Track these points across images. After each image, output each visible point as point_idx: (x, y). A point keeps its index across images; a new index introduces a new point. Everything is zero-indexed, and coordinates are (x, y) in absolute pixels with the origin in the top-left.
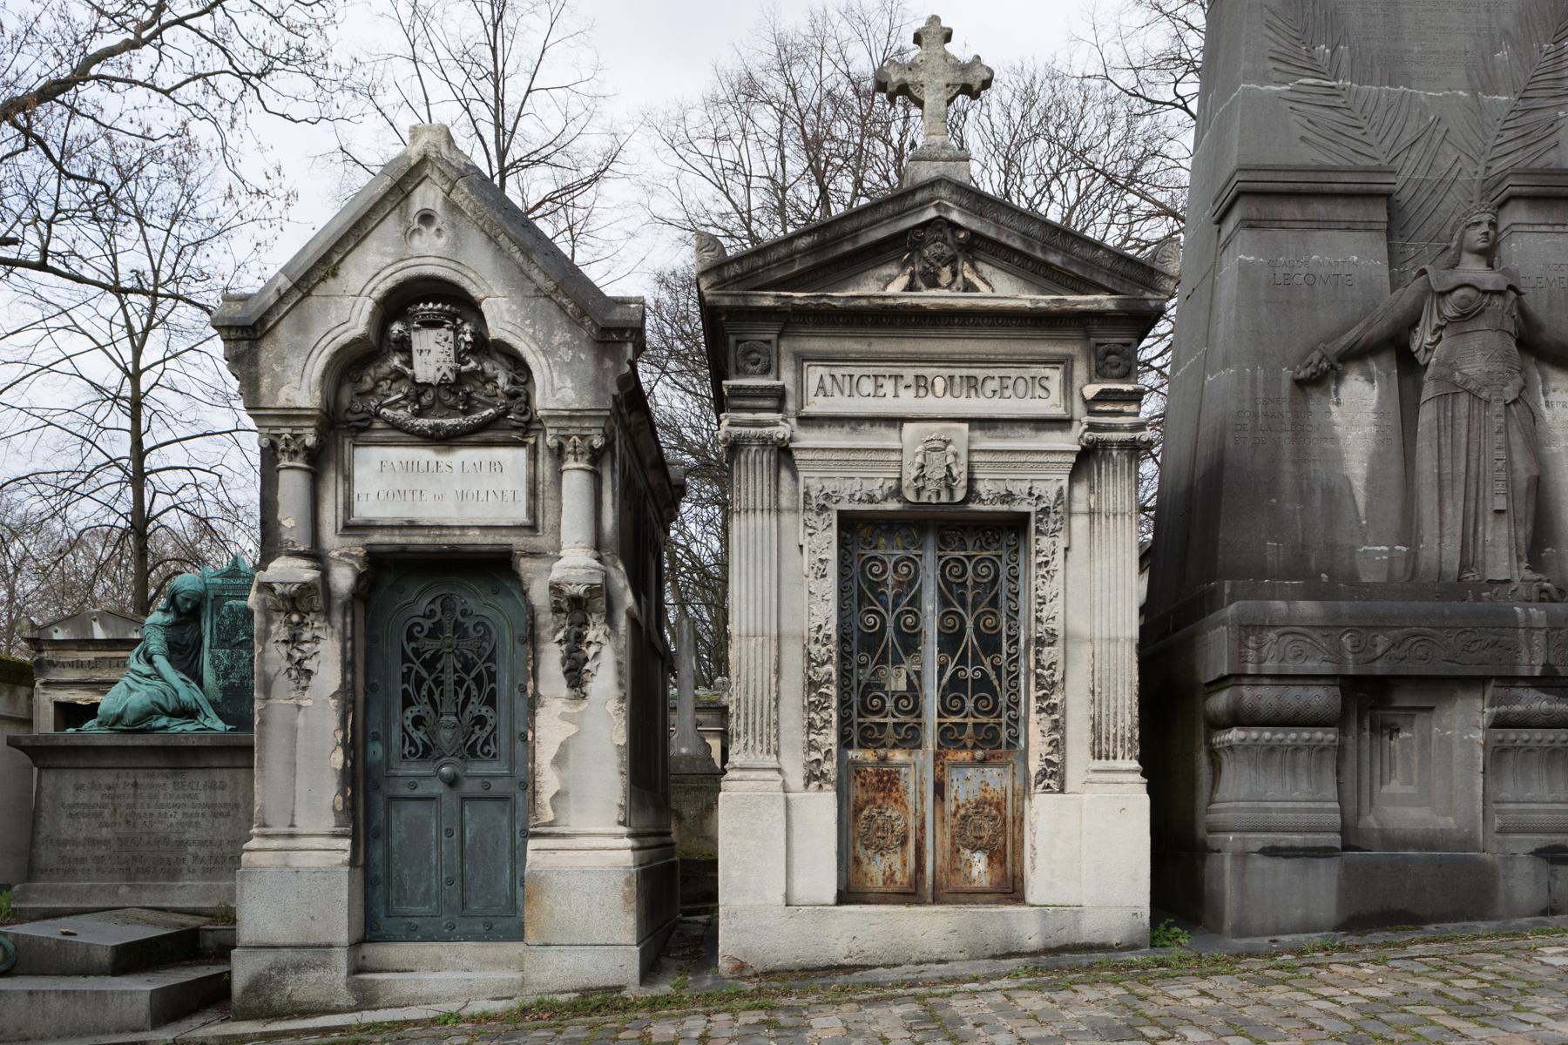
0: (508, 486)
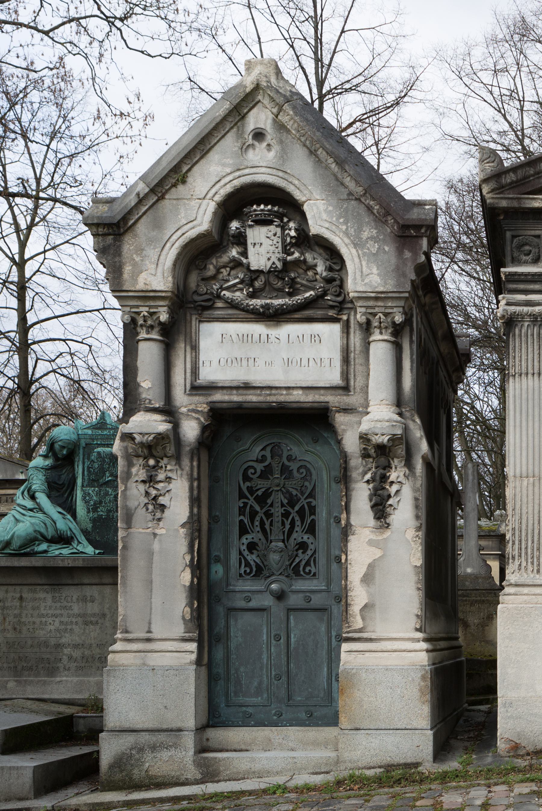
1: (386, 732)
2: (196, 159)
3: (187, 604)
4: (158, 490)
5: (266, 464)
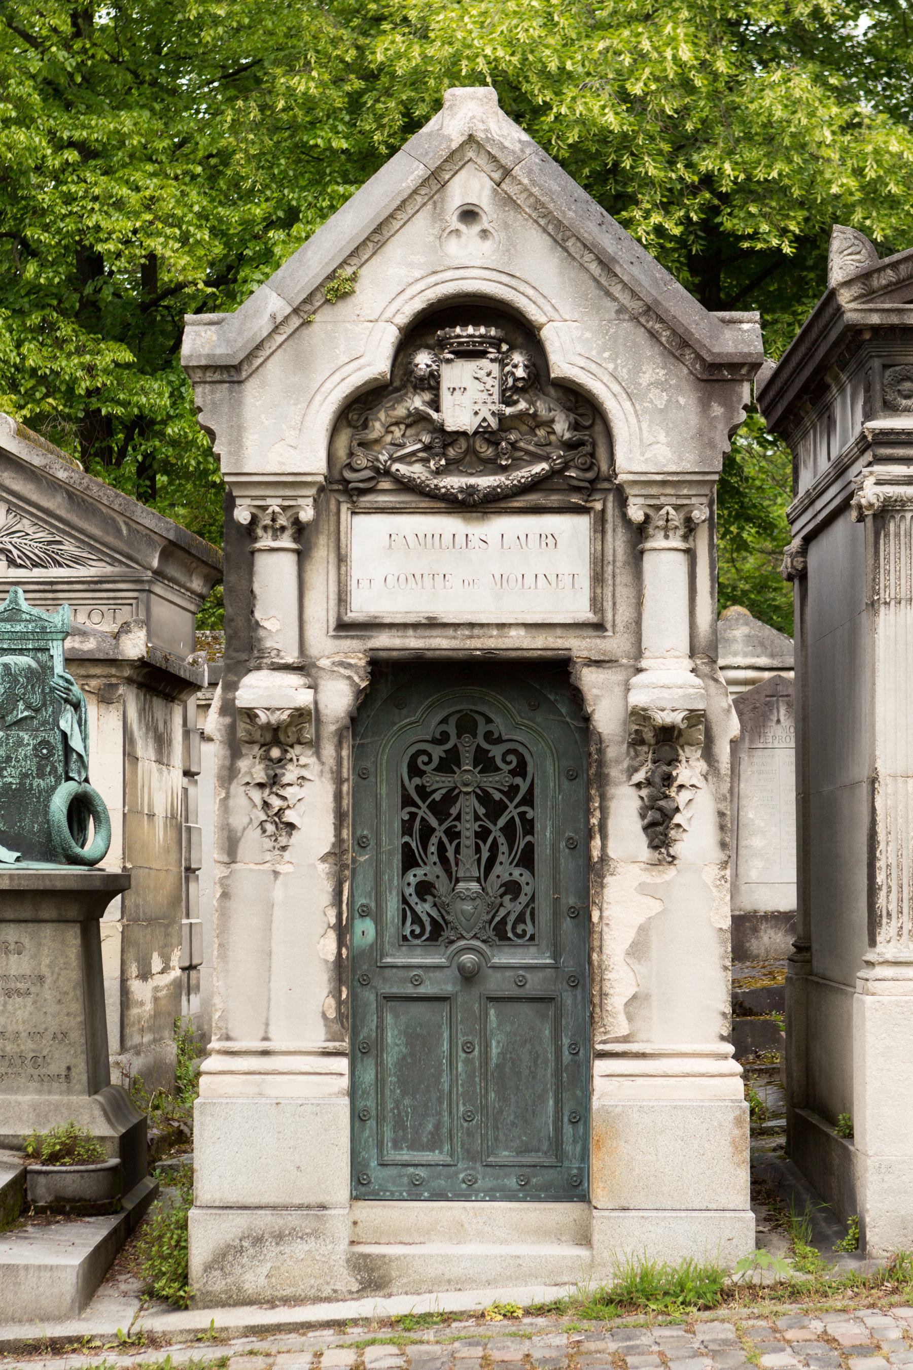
0: (565, 568)
1: (674, 1214)
2: (366, 257)
3: (330, 992)
4: (284, 798)
5: (448, 746)
